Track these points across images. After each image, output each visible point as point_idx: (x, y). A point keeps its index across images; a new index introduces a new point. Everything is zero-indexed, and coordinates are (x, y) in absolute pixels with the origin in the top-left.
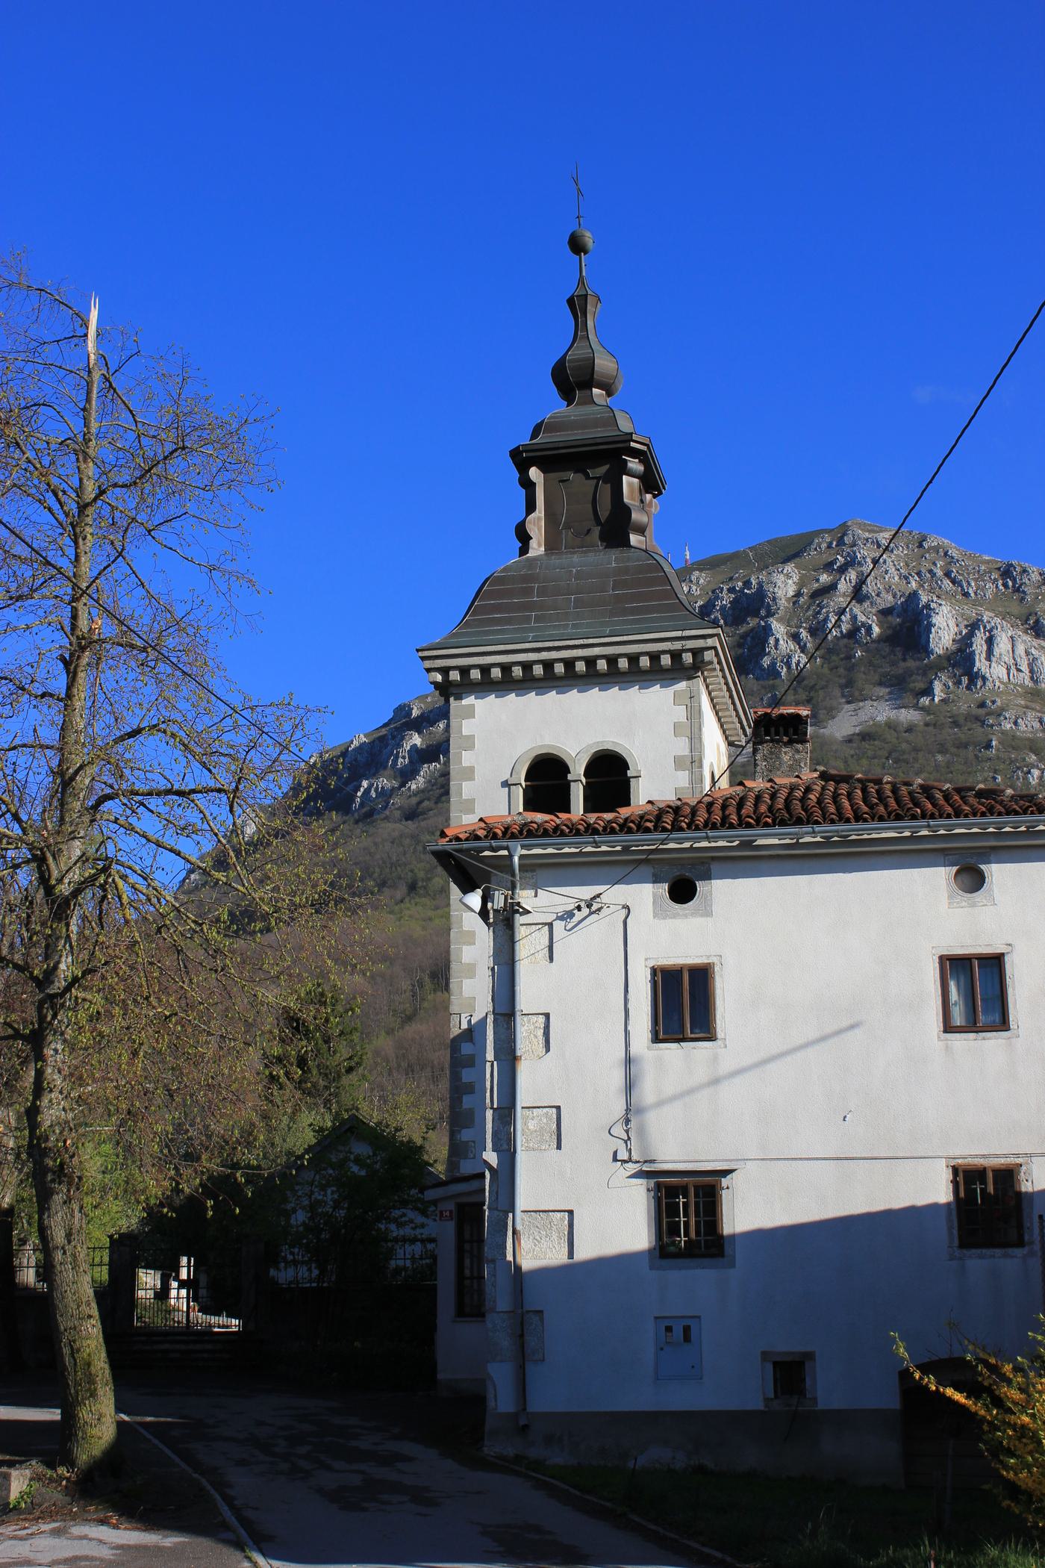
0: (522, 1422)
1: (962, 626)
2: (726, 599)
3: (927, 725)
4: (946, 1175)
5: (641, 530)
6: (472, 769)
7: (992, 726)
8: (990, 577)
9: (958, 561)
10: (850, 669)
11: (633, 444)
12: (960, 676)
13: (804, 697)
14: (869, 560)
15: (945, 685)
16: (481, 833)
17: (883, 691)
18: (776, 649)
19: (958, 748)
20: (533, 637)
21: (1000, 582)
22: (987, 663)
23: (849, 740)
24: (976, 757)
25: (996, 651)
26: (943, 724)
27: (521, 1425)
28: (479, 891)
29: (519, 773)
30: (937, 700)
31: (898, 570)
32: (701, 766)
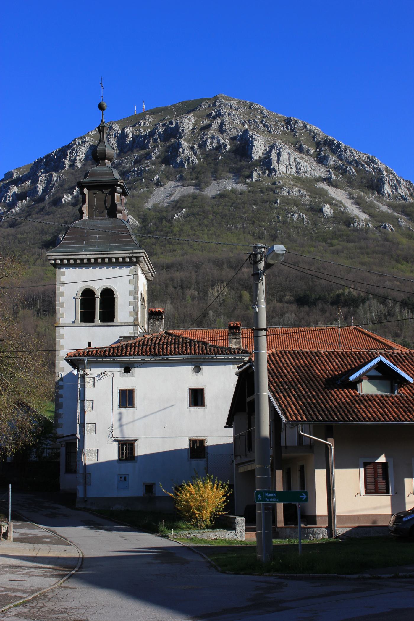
0: (85, 500)
1: (267, 147)
2: (161, 129)
3: (249, 191)
4: (188, 441)
5: (120, 212)
6: (63, 293)
7: (278, 193)
8: (280, 124)
9: (266, 116)
10: (216, 164)
11: (118, 183)
12: (265, 170)
13: (195, 177)
14: (226, 114)
15: (258, 173)
16: (77, 355)
17: (231, 175)
18: (183, 154)
19: (263, 203)
20: (85, 250)
21: (285, 127)
22: (277, 164)
23: (214, 197)
24: (270, 207)
25: (282, 159)
26: (256, 192)
27: (85, 500)
28: (76, 370)
29: (79, 295)
30: (254, 180)
31: (240, 119)
32: (137, 294)
